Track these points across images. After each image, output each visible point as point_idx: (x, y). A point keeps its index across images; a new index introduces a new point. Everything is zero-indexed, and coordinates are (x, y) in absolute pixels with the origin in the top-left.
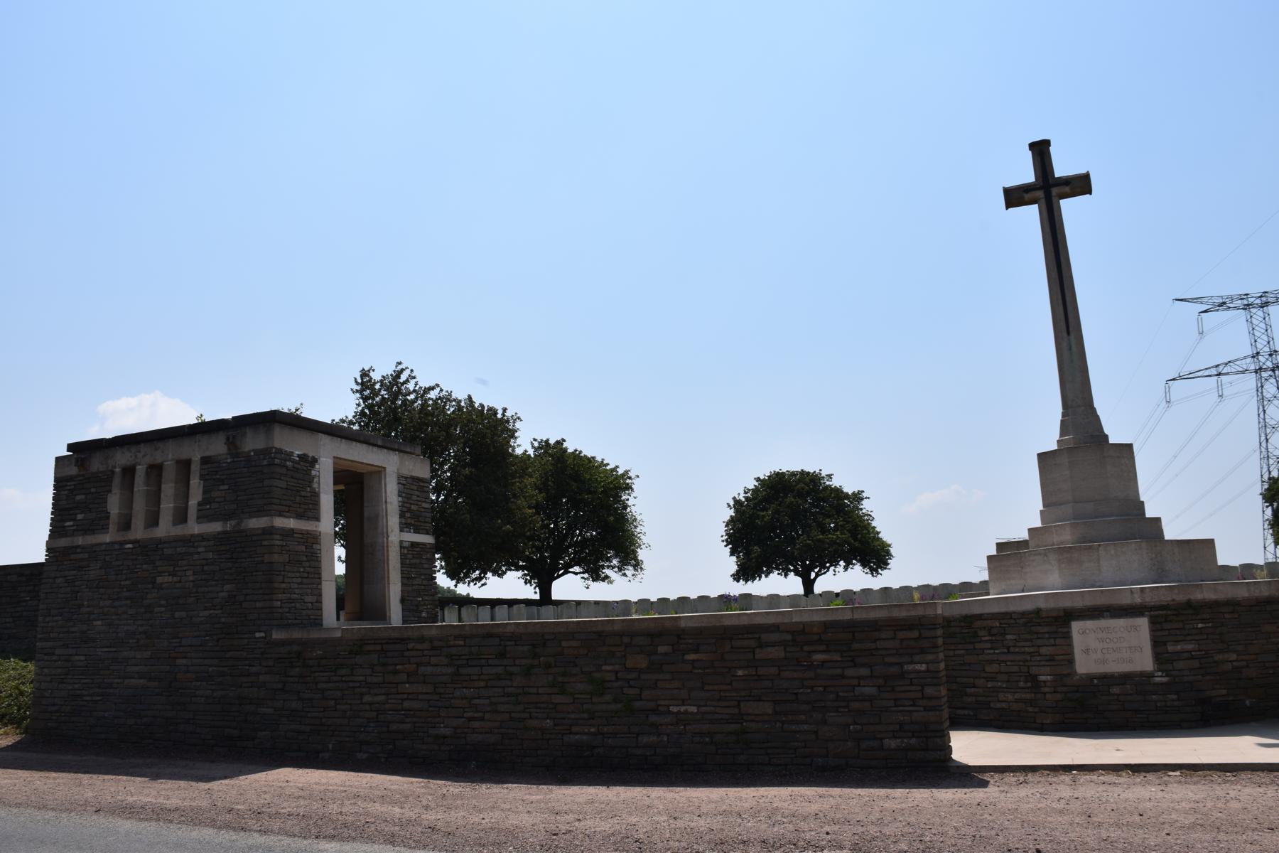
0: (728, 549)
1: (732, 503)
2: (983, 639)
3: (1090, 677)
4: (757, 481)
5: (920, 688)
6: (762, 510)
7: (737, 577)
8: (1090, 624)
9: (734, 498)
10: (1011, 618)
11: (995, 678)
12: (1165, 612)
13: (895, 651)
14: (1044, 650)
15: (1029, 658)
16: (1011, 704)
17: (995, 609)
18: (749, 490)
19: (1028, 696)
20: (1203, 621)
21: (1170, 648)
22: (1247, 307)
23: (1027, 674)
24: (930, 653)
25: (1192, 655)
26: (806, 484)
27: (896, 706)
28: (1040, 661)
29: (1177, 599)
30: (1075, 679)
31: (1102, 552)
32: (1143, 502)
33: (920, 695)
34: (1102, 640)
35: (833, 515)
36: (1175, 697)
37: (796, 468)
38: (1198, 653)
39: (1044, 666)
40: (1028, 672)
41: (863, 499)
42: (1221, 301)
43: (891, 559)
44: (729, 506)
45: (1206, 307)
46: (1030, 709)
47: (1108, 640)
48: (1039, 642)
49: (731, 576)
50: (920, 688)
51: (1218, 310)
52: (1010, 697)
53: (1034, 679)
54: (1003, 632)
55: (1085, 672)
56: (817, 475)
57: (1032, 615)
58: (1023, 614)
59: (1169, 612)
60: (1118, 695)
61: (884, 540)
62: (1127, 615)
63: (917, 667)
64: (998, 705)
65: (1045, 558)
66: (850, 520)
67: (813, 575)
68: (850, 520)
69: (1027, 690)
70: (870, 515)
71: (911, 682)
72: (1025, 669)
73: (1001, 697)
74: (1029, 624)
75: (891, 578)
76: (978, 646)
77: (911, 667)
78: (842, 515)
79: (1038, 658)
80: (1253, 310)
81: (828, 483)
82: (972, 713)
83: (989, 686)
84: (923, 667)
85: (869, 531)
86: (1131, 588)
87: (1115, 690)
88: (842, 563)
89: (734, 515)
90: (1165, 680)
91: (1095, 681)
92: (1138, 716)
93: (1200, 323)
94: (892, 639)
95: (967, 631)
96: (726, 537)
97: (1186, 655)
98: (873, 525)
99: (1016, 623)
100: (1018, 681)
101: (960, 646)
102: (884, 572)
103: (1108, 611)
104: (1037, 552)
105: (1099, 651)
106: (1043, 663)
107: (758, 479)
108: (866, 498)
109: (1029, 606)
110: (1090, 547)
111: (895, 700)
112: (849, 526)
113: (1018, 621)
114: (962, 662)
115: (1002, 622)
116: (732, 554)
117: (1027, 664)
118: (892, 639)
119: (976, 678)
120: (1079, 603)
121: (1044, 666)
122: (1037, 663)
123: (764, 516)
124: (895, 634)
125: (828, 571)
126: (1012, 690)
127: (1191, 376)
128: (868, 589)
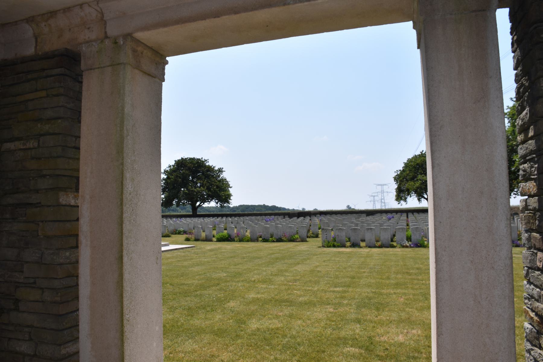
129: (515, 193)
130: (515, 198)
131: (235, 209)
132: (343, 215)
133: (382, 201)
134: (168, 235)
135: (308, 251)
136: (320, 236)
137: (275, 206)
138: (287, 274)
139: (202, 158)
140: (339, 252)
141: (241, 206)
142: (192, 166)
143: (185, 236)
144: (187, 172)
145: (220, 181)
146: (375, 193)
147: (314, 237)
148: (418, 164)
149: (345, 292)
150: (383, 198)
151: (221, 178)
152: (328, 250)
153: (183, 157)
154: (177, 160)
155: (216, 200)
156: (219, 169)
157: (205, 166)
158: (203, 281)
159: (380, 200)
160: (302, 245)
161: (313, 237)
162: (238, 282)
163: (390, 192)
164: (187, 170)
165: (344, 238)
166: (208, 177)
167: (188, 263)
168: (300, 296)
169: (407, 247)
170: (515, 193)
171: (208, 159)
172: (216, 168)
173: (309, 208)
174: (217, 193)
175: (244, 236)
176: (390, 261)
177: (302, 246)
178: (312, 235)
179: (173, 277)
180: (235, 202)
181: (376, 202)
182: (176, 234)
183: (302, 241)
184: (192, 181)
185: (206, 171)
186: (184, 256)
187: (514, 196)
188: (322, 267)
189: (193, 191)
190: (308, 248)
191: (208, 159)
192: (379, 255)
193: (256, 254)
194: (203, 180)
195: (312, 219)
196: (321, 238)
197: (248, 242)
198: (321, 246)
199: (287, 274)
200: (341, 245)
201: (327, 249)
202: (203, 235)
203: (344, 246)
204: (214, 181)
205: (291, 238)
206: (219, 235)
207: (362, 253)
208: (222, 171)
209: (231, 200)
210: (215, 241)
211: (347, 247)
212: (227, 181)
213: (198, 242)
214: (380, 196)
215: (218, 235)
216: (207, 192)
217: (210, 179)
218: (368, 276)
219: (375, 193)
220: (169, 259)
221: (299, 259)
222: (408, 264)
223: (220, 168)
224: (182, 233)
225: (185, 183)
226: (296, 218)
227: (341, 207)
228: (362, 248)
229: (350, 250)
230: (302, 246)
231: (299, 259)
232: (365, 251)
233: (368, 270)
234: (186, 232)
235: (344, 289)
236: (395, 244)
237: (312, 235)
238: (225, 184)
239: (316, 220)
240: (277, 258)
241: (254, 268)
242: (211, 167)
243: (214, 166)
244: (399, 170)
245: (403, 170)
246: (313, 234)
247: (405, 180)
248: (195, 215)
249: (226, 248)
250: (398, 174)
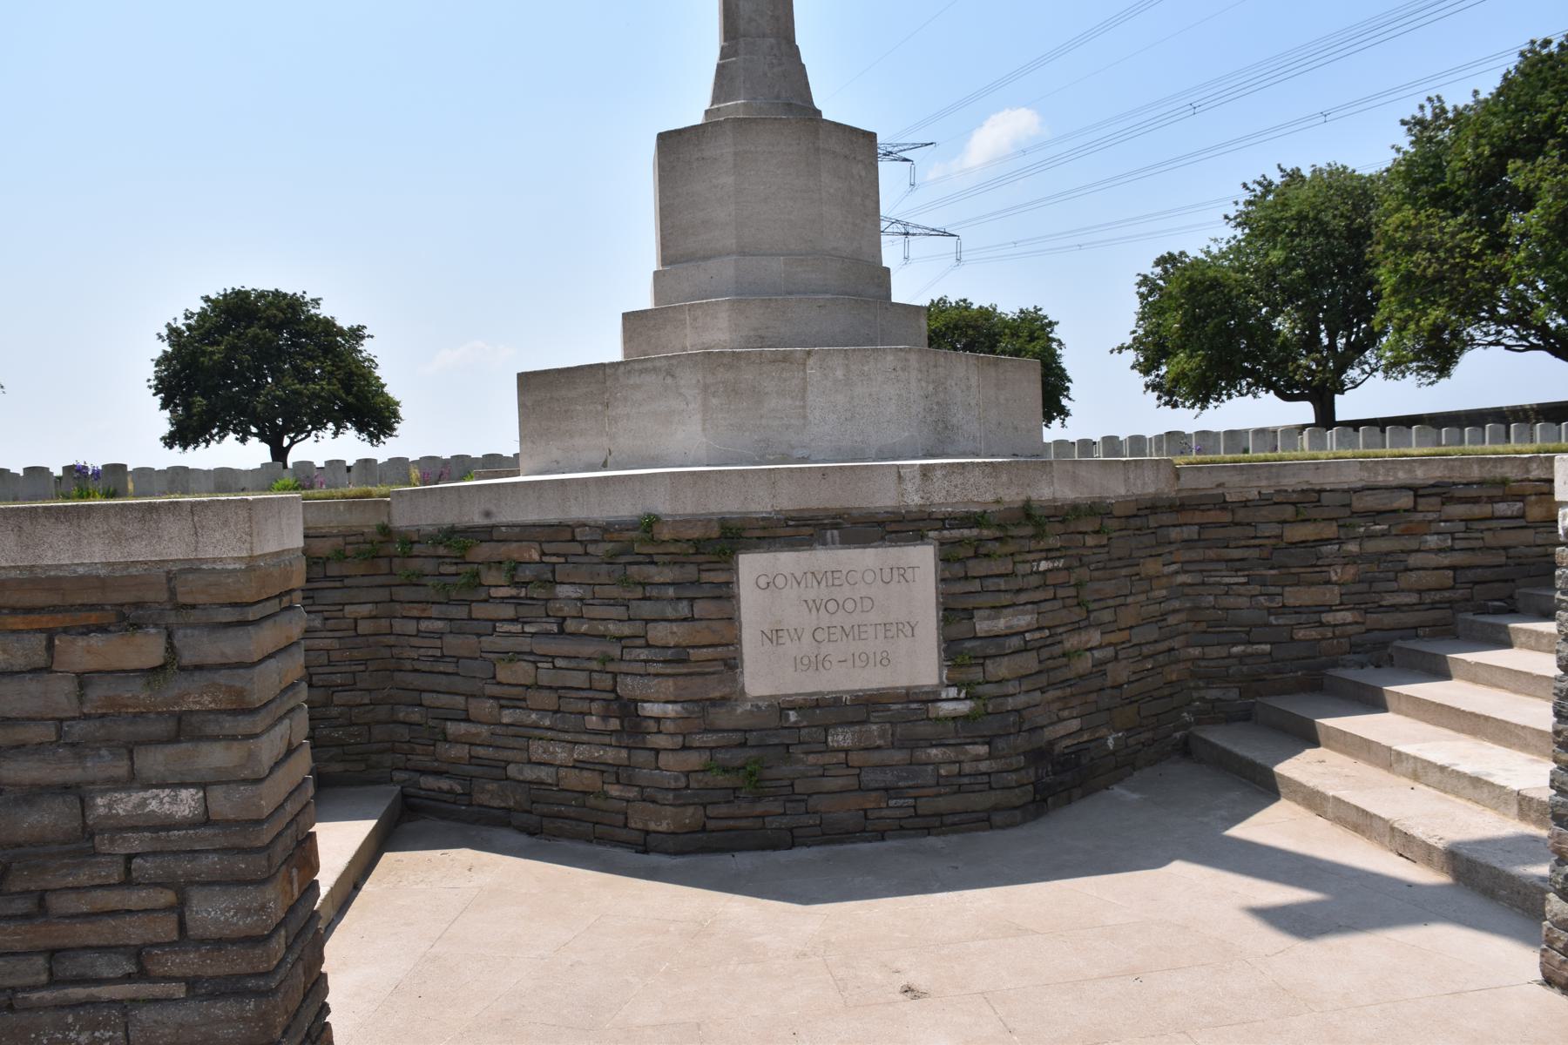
0: (157, 400)
1: (165, 332)
2: (494, 592)
3: (781, 706)
4: (206, 301)
5: (167, 897)
6: (211, 344)
7: (169, 441)
8: (787, 561)
9: (168, 325)
10: (573, 540)
11: (524, 700)
12: (975, 532)
13: (46, 733)
14: (658, 633)
15: (615, 651)
16: (563, 772)
17: (531, 515)
18: (193, 314)
19: (610, 755)
20: (1048, 553)
21: (983, 626)
23: (612, 696)
24: (215, 738)
25: (1026, 642)
26: (281, 310)
27: (54, 982)
28: (646, 661)
29: (1007, 499)
30: (739, 710)
31: (813, 371)
32: (888, 270)
33: (165, 929)
34: (816, 606)
35: (318, 357)
36: (983, 750)
37: (268, 286)
38: (1037, 635)
39: (657, 675)
40: (614, 691)
41: (363, 338)
43: (398, 422)
44: (160, 337)
46: (615, 791)
47: (832, 606)
48: (647, 610)
49: (161, 439)
50: (167, 897)
52: (561, 754)
53: (627, 710)
54: (549, 576)
55: (766, 692)
56: (298, 299)
57: (633, 534)
58: (607, 530)
59: (986, 533)
60: (847, 751)
61: (391, 395)
62: (883, 539)
63: (153, 805)
64: (530, 773)
65: (669, 380)
66: (343, 364)
67: (286, 442)
68: (343, 364)
69: (607, 740)
70: (373, 361)
71: (128, 870)
72: (607, 682)
73: (537, 751)
74: (624, 559)
75: (406, 443)
76: (480, 611)
77: (125, 804)
78: (330, 356)
79: (644, 654)
81: (313, 311)
82: (458, 789)
83: (505, 720)
84: (186, 803)
85: (369, 383)
86: (898, 466)
87: (841, 738)
88: (330, 425)
89: (169, 349)
90: (963, 707)
91: (793, 716)
92: (892, 803)
94: (35, 671)
95: (453, 569)
96: (155, 382)
97: (1015, 642)
98: (377, 375)
99: (586, 554)
100: (583, 714)
101: (434, 611)
102: (389, 440)
103: (835, 526)
104: (649, 365)
105: (806, 637)
106: (658, 668)
107: (207, 299)
108: (368, 336)
109: (624, 509)
110: (786, 358)
111: (53, 953)
112: (340, 374)
113: (591, 549)
114: (438, 653)
115: (547, 548)
116: (164, 406)
117: (611, 667)
118: (35, 671)
119: (473, 696)
120: (761, 504)
121: (657, 675)
122: (638, 668)
123: (213, 353)
124: (50, 646)
125: (308, 436)
126: (568, 737)
128: (338, 461)
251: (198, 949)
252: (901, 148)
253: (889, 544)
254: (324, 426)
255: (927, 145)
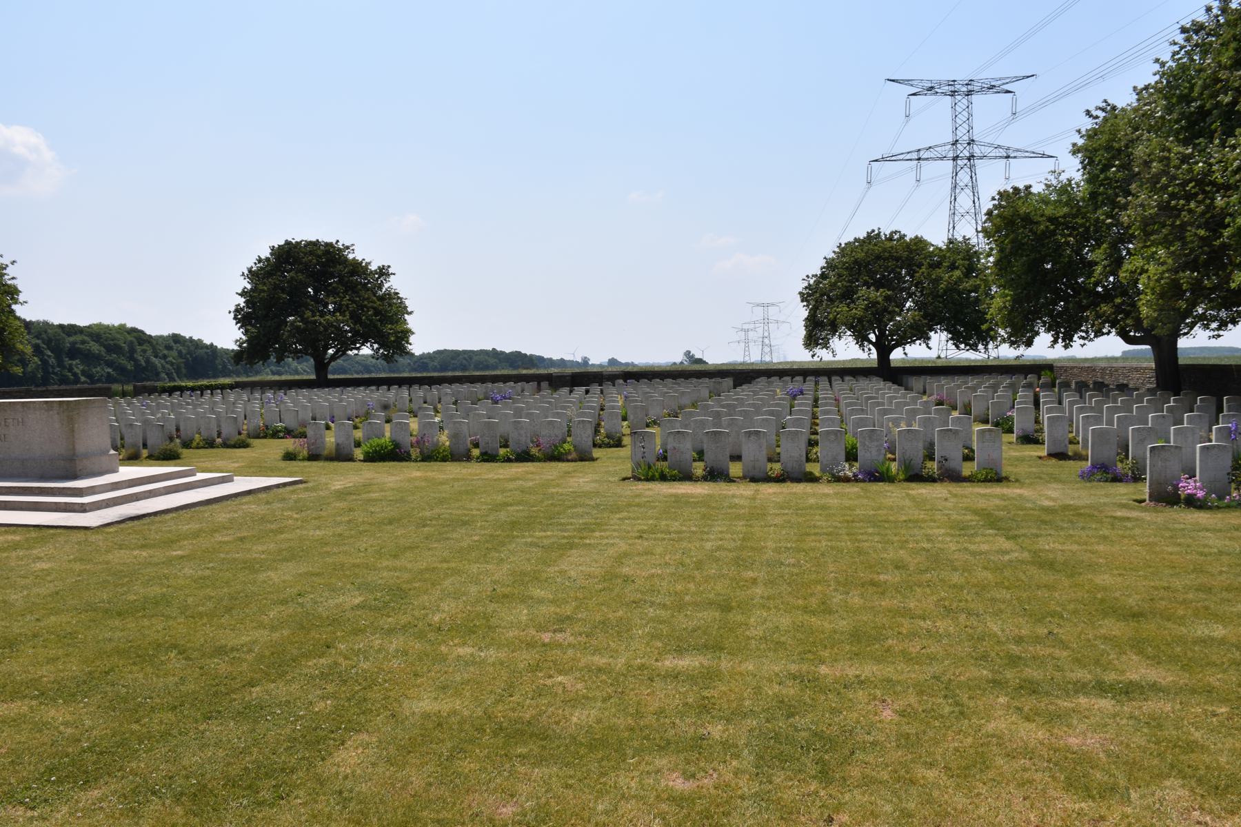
1: (246, 272)
22: (953, 94)
42: (930, 85)
45: (914, 90)
51: (926, 94)
80: (959, 98)
93: (908, 105)
127: (893, 158)
129: (1084, 334)
130: (1082, 346)
131: (425, 361)
132: (679, 381)
133: (765, 342)
134: (243, 442)
135: (597, 493)
136: (626, 440)
137: (520, 352)
138: (538, 593)
139: (338, 241)
140: (678, 500)
141: (439, 353)
142: (315, 261)
143: (289, 444)
144: (301, 277)
145: (382, 298)
146: (749, 323)
147: (610, 447)
148: (856, 262)
149: (709, 676)
150: (766, 334)
151: (386, 290)
152: (649, 489)
153: (290, 239)
154: (276, 246)
155: (374, 343)
156: (379, 267)
157: (346, 259)
158: (286, 632)
159: (761, 340)
160: (581, 472)
161: (609, 446)
162: (391, 631)
163: (784, 322)
164: (301, 271)
165: (686, 449)
166: (352, 288)
167: (265, 548)
168: (575, 701)
169: (847, 480)
170: (1084, 334)
171: (353, 245)
172: (373, 267)
173: (598, 358)
174: (375, 326)
175: (437, 444)
176: (815, 534)
177: (581, 475)
178: (606, 440)
179: (201, 615)
180: (420, 345)
181: (751, 344)
182: (265, 437)
183: (582, 460)
184: (315, 298)
185: (347, 273)
186: (263, 520)
187: (1082, 342)
188: (637, 559)
189: (315, 322)
190: (593, 485)
191: (353, 245)
192: (783, 511)
193: (458, 508)
194: (341, 295)
195: (605, 392)
196: (629, 446)
197: (445, 461)
198: (630, 475)
199: (538, 593)
200: (681, 475)
201: (646, 487)
202: (330, 439)
203: (687, 477)
204: (368, 299)
205: (553, 451)
206: (371, 445)
207: (737, 501)
208: (388, 275)
209: (410, 344)
210: (360, 461)
211: (697, 480)
212: (401, 299)
213: (315, 463)
214: (760, 330)
215: (368, 445)
216: (352, 325)
217: (357, 292)
218: (769, 598)
219: (749, 323)
220: (216, 531)
221: (571, 524)
222: (866, 544)
223: (383, 266)
224: (281, 434)
225: (297, 303)
226: (566, 390)
227: (667, 355)
228: (734, 481)
229: (706, 492)
230: (580, 477)
231: (571, 524)
232: (745, 491)
233: (762, 575)
234: (292, 431)
235: (706, 663)
236: (815, 469)
237: (606, 440)
238: (396, 304)
239: (616, 398)
240: (514, 525)
241: (445, 565)
242: (362, 262)
243: (367, 260)
244: (813, 276)
245: (823, 274)
246: (608, 437)
247: (827, 300)
248: (322, 381)
249: (384, 483)
250: (809, 284)
251: (1206, 327)
252: (1004, 81)
253: (1096, 364)
254: (911, 240)
255: (1028, 77)
